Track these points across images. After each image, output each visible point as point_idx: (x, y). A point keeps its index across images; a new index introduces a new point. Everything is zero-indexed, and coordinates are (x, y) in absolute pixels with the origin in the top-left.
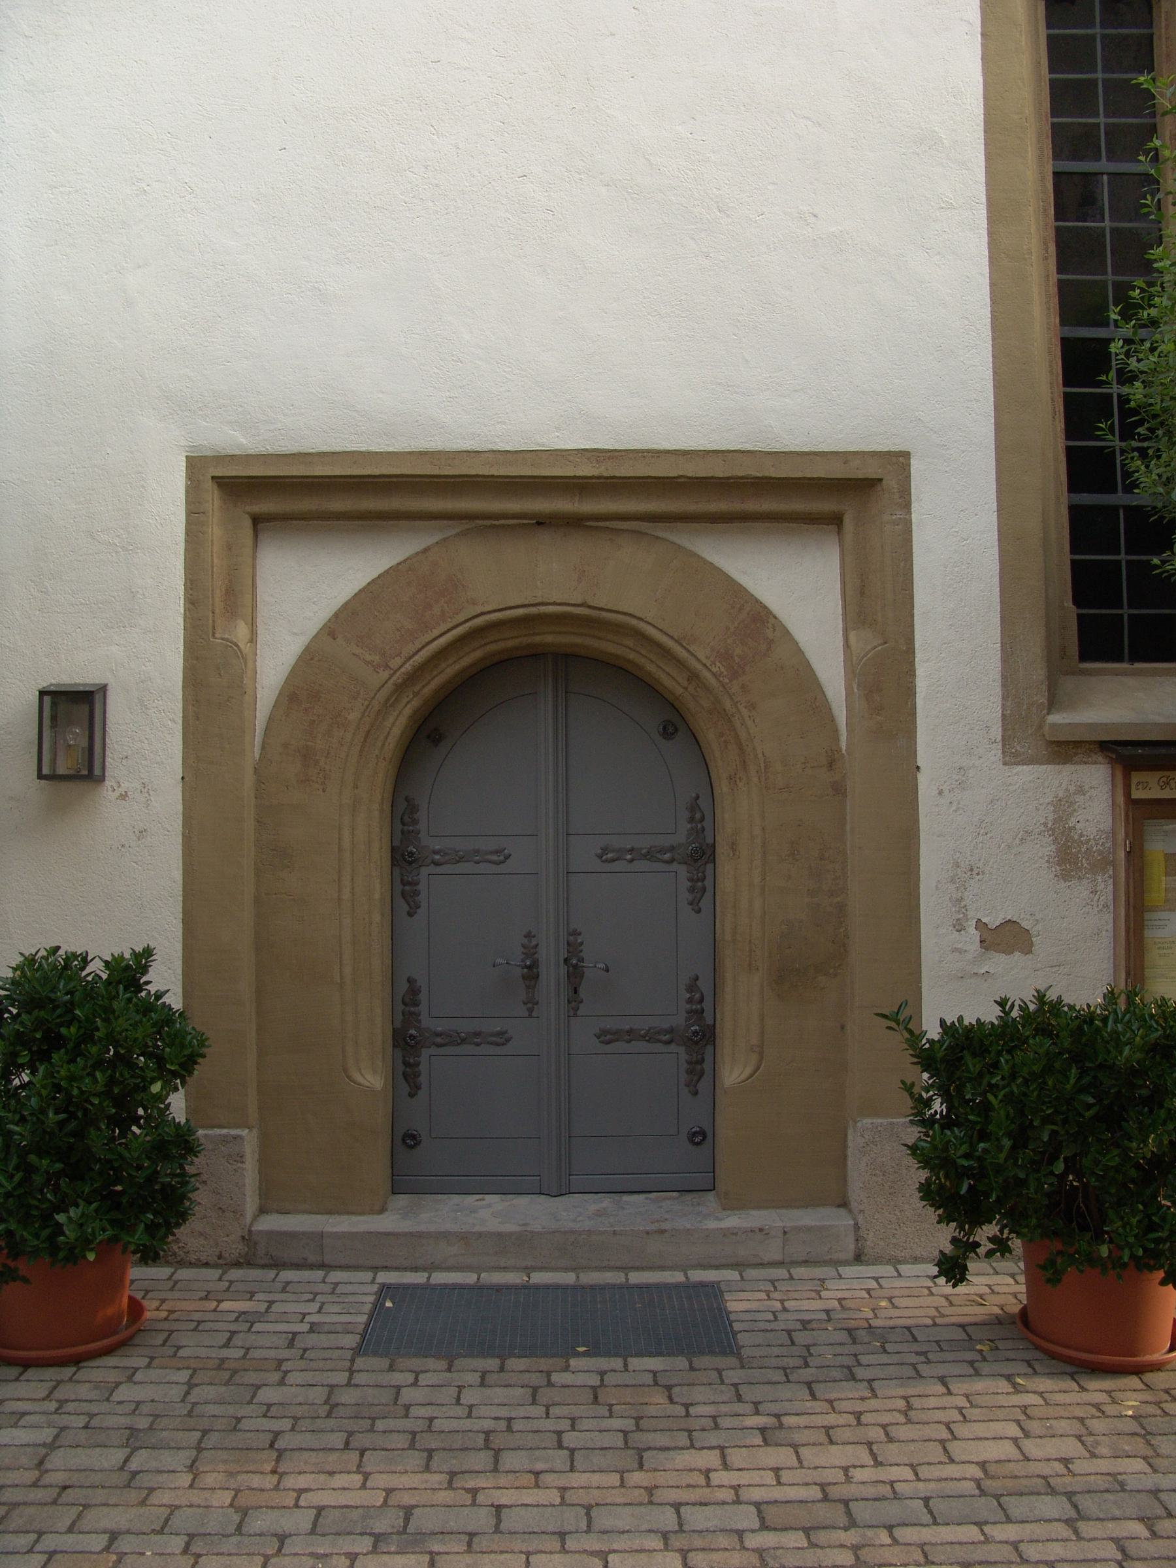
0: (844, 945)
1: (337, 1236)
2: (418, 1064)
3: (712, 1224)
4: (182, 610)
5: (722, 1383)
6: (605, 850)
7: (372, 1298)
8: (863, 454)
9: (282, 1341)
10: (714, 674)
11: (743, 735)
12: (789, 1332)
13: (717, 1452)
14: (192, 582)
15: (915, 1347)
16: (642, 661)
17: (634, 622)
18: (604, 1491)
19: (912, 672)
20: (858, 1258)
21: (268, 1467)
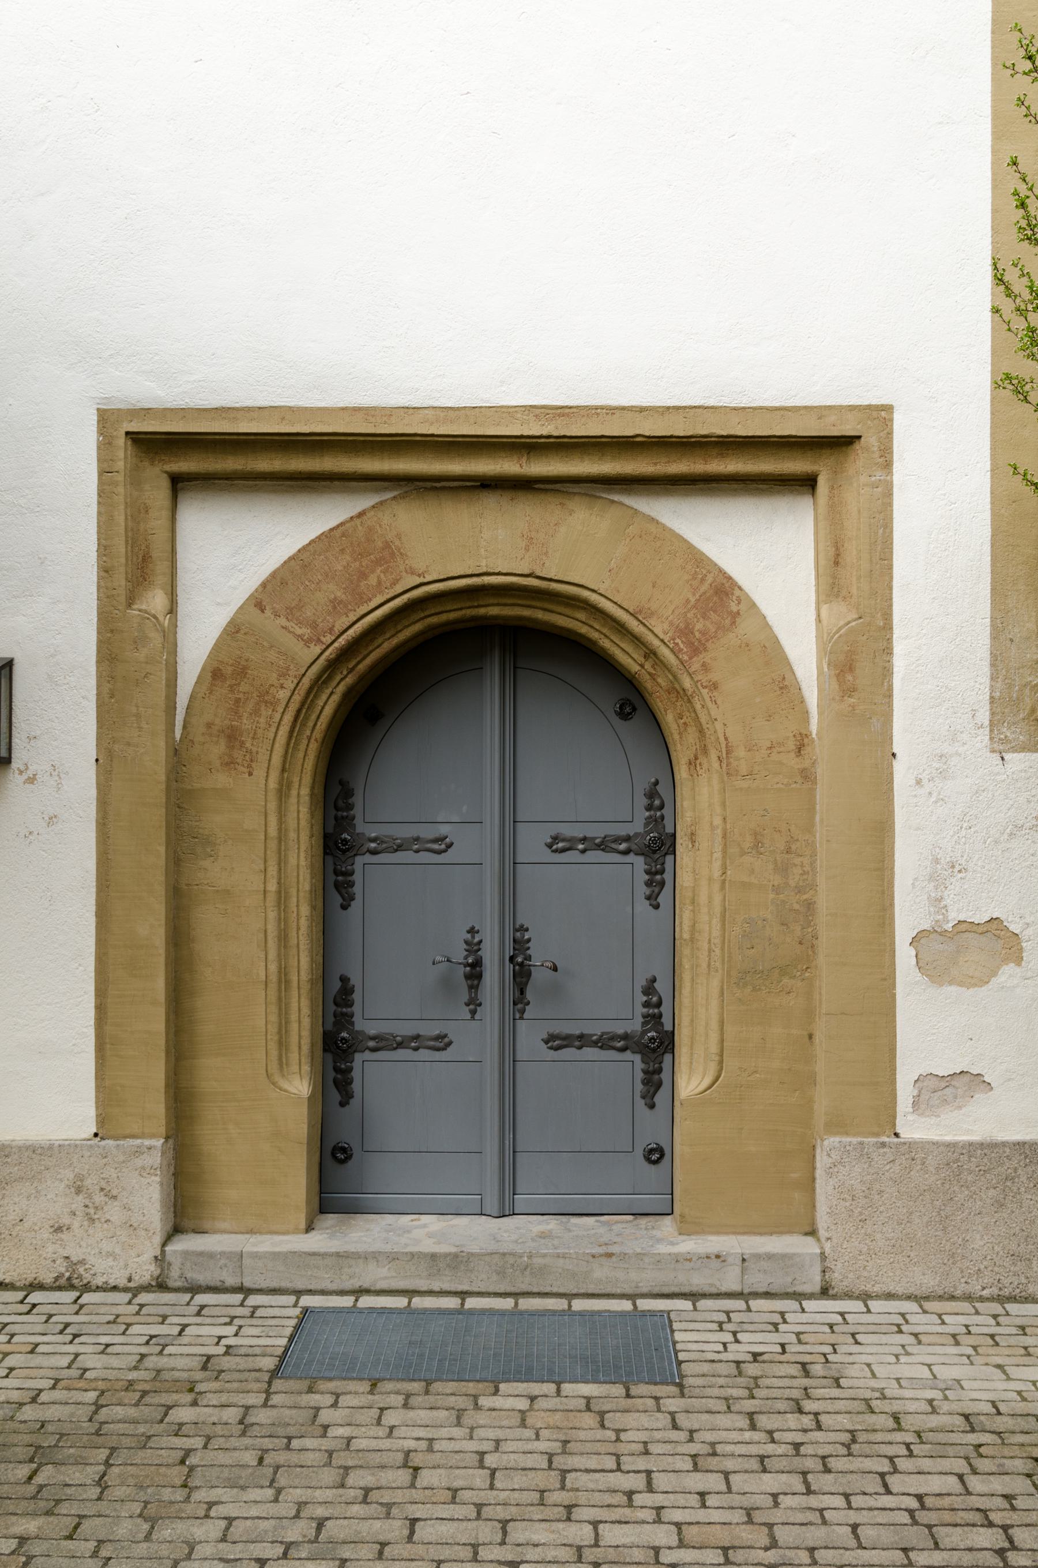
0: (813, 946)
1: (255, 1256)
2: (351, 1069)
3: (663, 1249)
4: (95, 579)
5: (659, 1410)
6: (556, 839)
7: (293, 1322)
8: (840, 408)
10: (672, 650)
11: (703, 718)
12: (738, 1363)
13: (644, 1475)
14: (105, 547)
16: (594, 635)
17: (586, 594)
18: (523, 1508)
19: (888, 651)
20: (825, 1292)
21: (178, 1482)
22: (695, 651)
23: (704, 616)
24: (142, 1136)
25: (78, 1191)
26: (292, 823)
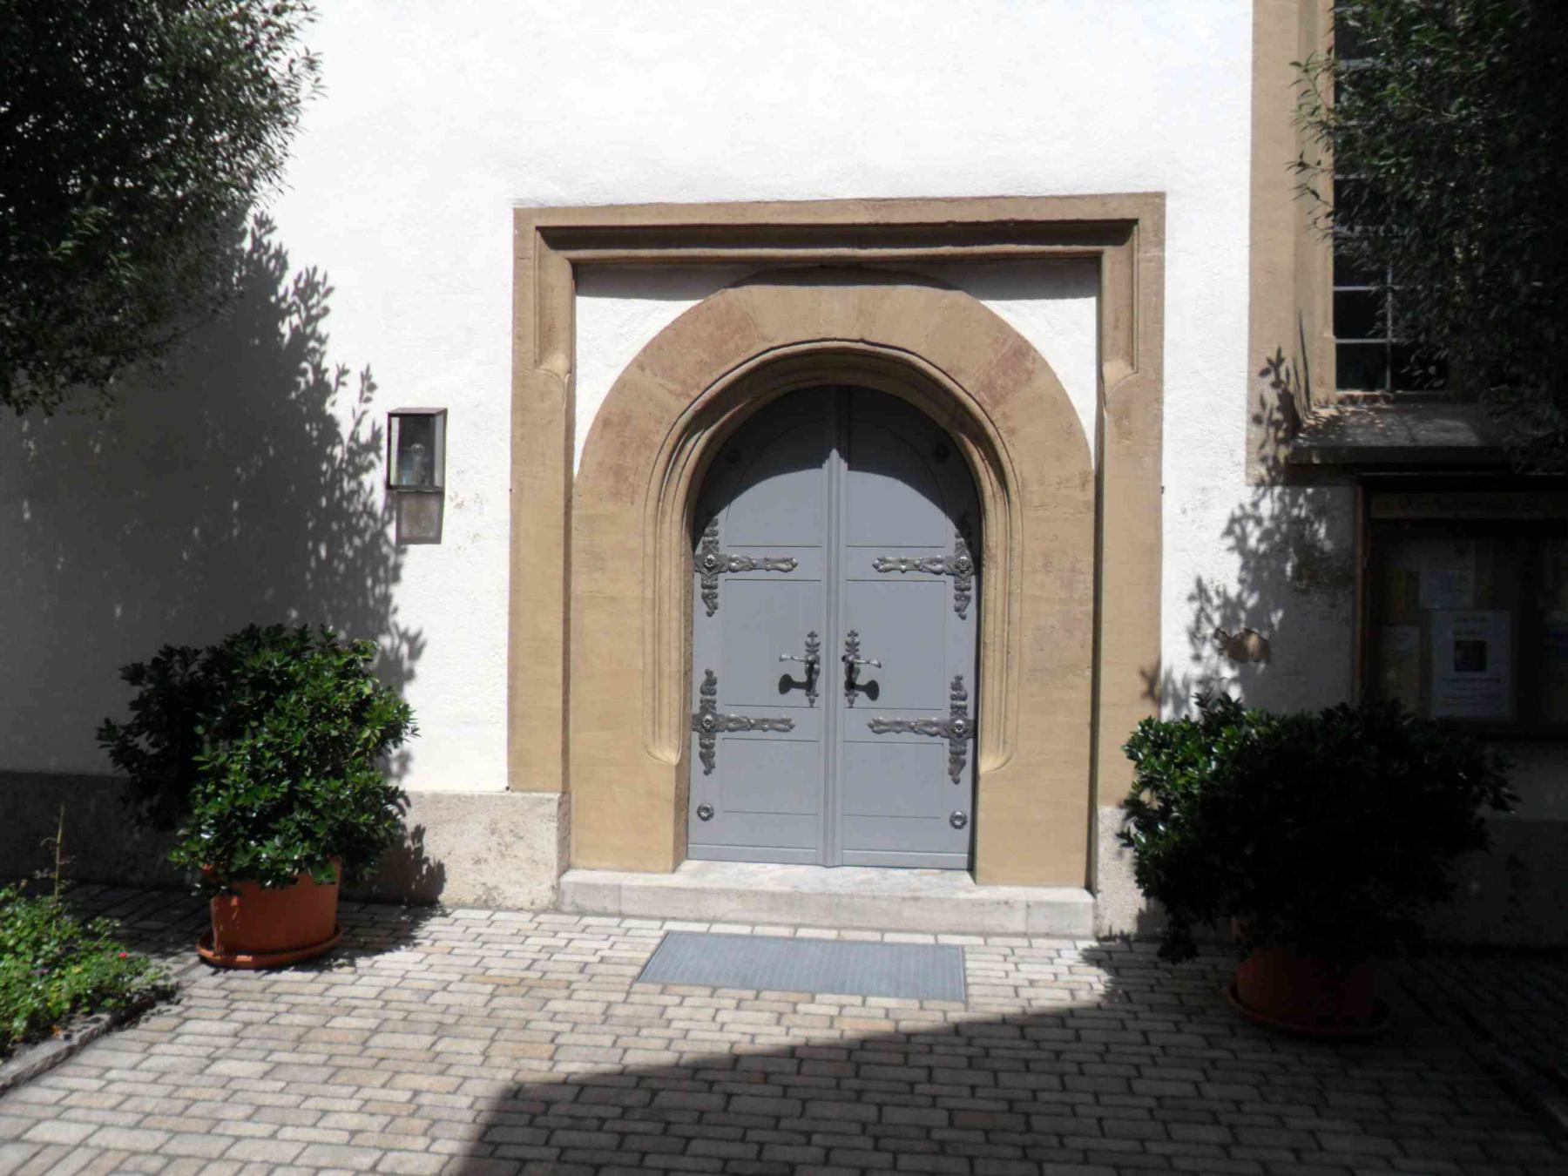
1: (631, 889)
3: (962, 895)
7: (657, 941)
9: (574, 968)
15: (1129, 1007)
21: (546, 1055)
22: (996, 403)
23: (1005, 373)
24: (544, 791)
25: (493, 832)
26: (666, 545)
